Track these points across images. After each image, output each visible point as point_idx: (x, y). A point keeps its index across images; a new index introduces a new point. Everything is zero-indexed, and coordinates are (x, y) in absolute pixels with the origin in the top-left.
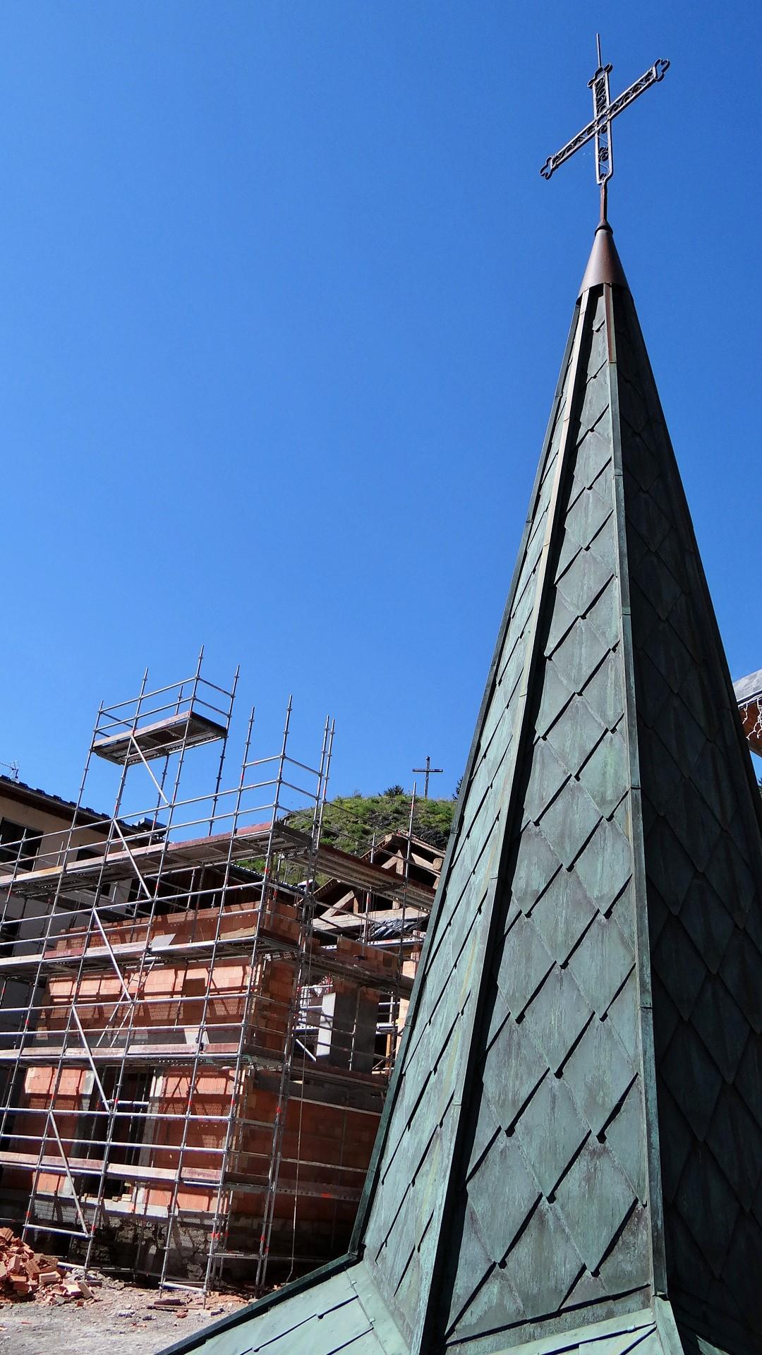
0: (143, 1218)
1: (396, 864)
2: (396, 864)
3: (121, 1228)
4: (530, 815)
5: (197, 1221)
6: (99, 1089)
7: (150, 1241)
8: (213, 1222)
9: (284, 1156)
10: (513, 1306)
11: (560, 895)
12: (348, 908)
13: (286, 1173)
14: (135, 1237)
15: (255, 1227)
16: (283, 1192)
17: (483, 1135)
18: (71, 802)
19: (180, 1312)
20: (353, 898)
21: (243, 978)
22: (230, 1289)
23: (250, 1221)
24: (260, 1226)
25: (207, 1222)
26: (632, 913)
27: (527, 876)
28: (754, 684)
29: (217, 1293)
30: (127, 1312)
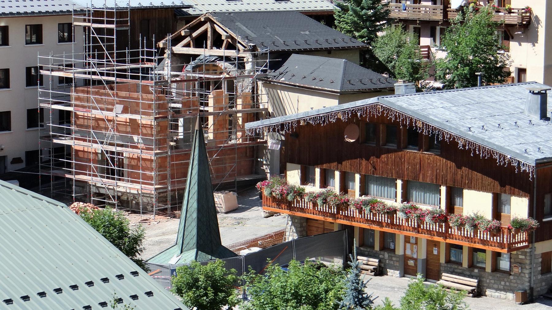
0: (130, 193)
1: (207, 28)
2: (207, 28)
3: (122, 196)
4: (188, 209)
5: (148, 195)
6: (108, 160)
7: (132, 200)
8: (154, 196)
9: (171, 179)
10: (187, 249)
11: (191, 217)
12: (188, 45)
13: (173, 183)
14: (128, 198)
15: (165, 195)
16: (172, 188)
17: (185, 238)
18: (53, 11)
19: (149, 224)
20: (190, 40)
21: (164, 268)
22: (161, 214)
23: (164, 194)
24: (167, 195)
25: (151, 196)
26: (196, 220)
27: (188, 215)
28: (253, 124)
29: (157, 215)
30: (134, 224)
